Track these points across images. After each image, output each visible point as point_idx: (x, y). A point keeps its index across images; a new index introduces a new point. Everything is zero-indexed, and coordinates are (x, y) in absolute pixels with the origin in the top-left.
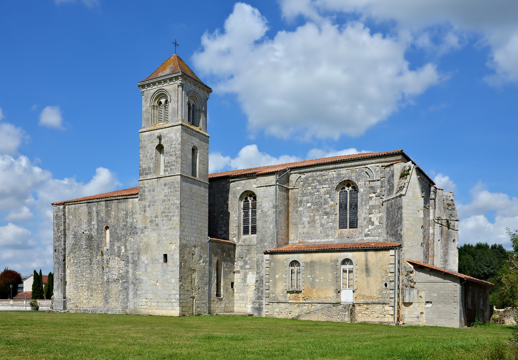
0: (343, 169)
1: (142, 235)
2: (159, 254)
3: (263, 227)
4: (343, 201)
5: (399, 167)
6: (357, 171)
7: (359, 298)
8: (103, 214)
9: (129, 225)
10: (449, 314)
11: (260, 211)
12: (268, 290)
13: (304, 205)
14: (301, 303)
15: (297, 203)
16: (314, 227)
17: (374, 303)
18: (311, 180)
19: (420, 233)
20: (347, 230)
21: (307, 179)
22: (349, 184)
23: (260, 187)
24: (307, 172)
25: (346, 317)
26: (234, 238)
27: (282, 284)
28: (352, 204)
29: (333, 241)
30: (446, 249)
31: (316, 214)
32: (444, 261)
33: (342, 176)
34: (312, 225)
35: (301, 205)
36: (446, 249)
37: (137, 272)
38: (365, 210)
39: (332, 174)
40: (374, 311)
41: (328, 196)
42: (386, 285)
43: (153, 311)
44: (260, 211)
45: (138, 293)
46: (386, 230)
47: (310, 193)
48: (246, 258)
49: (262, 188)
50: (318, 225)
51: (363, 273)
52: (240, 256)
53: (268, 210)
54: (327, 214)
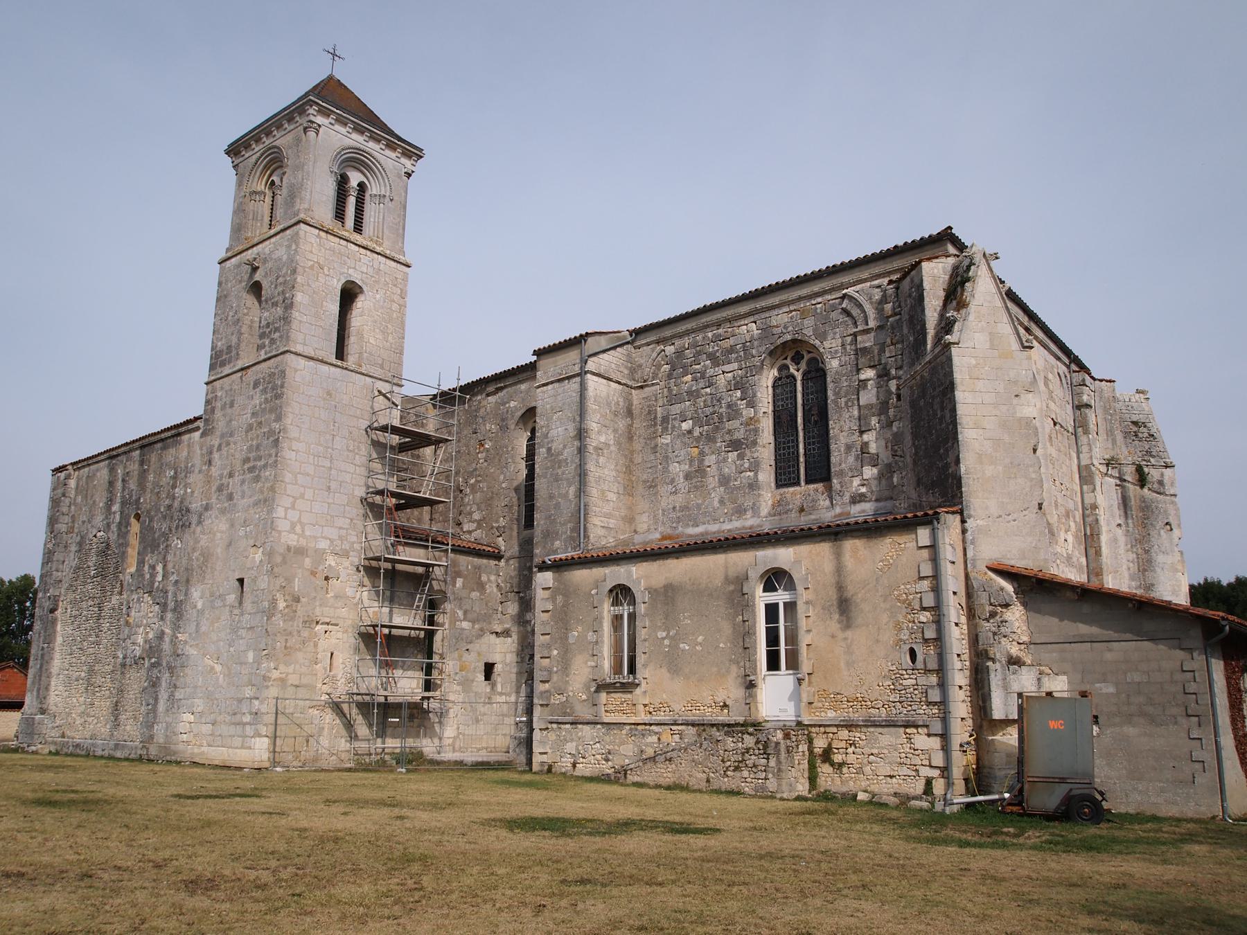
0: (776, 312)
1: (199, 529)
2: (227, 579)
3: (551, 497)
4: (783, 406)
5: (941, 272)
6: (819, 311)
7: (820, 705)
8: (133, 485)
9: (176, 504)
10: (1172, 765)
11: (544, 450)
12: (548, 681)
13: (673, 427)
14: (638, 724)
15: (655, 424)
17: (874, 721)
18: (692, 355)
19: (1031, 469)
20: (797, 488)
21: (680, 353)
22: (798, 353)
24: (681, 336)
25: (770, 776)
26: (501, 539)
28: (810, 410)
29: (755, 524)
30: (1145, 550)
31: (707, 450)
32: (1141, 588)
33: (776, 331)
35: (665, 429)
36: (1145, 550)
37: (179, 635)
38: (848, 422)
39: (749, 329)
41: (739, 393)
42: (913, 653)
43: (203, 749)
44: (544, 450)
45: (178, 695)
47: (689, 393)
49: (550, 387)
50: (712, 482)
51: (831, 614)
52: (512, 587)
53: (565, 447)
54: (735, 445)
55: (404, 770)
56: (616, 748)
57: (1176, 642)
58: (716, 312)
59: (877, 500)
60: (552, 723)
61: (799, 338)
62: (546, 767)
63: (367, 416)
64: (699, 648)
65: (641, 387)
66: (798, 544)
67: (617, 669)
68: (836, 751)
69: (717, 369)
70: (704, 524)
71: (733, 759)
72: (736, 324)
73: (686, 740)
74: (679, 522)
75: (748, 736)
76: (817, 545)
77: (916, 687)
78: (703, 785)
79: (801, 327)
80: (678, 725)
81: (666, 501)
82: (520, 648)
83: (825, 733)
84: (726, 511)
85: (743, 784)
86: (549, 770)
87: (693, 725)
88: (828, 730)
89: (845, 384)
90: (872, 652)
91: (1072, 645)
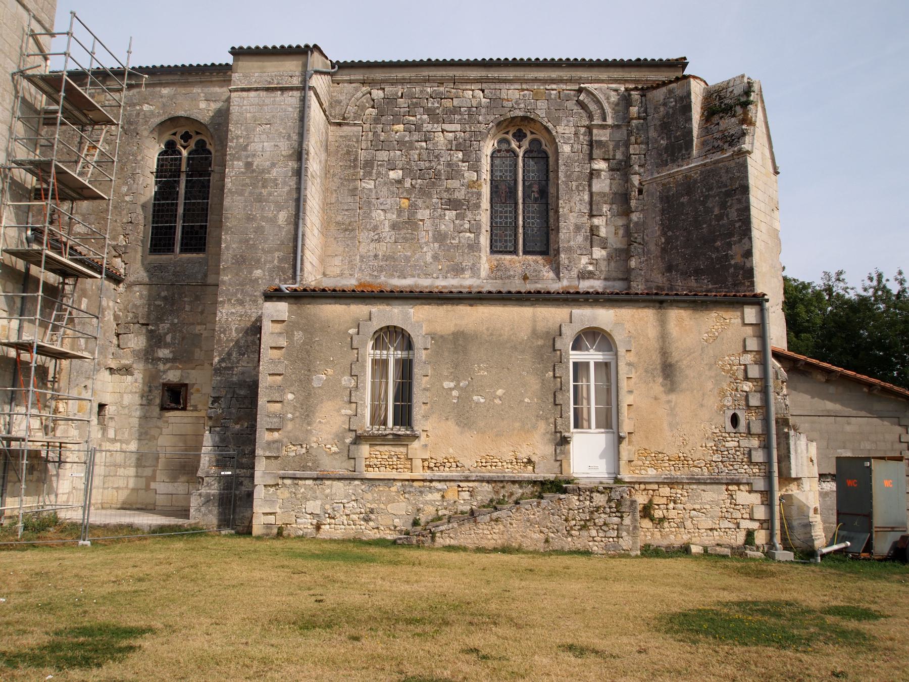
0: (508, 86)
3: (250, 218)
4: (501, 177)
6: (553, 96)
11: (241, 163)
12: (278, 430)
14: (413, 481)
15: (355, 167)
16: (412, 240)
17: (699, 479)
18: (406, 105)
21: (390, 100)
22: (520, 130)
23: (243, 90)
24: (394, 83)
25: (624, 534)
27: (338, 411)
31: (420, 202)
33: (505, 104)
34: (405, 234)
35: (368, 174)
38: (578, 205)
39: (472, 95)
40: (697, 507)
41: (460, 155)
42: (735, 420)
44: (241, 163)
46: (663, 258)
48: (161, 325)
49: (252, 94)
50: (425, 235)
51: (654, 377)
52: (136, 317)
54: (454, 204)
55: (88, 543)
56: (382, 506)
57: (896, 420)
58: (441, 68)
59: (605, 279)
60: (283, 478)
61: (532, 117)
62: (275, 531)
63: (15, 56)
64: (497, 401)
65: (339, 124)
66: (619, 307)
67: (378, 418)
68: (657, 507)
69: (436, 125)
70: (414, 277)
71: (578, 518)
72: (461, 87)
73: (479, 498)
74: (382, 271)
75: (598, 494)
76: (640, 310)
77: (738, 449)
78: (541, 546)
79: (533, 107)
80: (469, 481)
81: (366, 247)
82: (146, 389)
83: (645, 489)
84: (440, 267)
85: (591, 543)
86: (280, 534)
87: (488, 482)
88: (648, 487)
89: (577, 169)
90: (696, 415)
91: (821, 418)
